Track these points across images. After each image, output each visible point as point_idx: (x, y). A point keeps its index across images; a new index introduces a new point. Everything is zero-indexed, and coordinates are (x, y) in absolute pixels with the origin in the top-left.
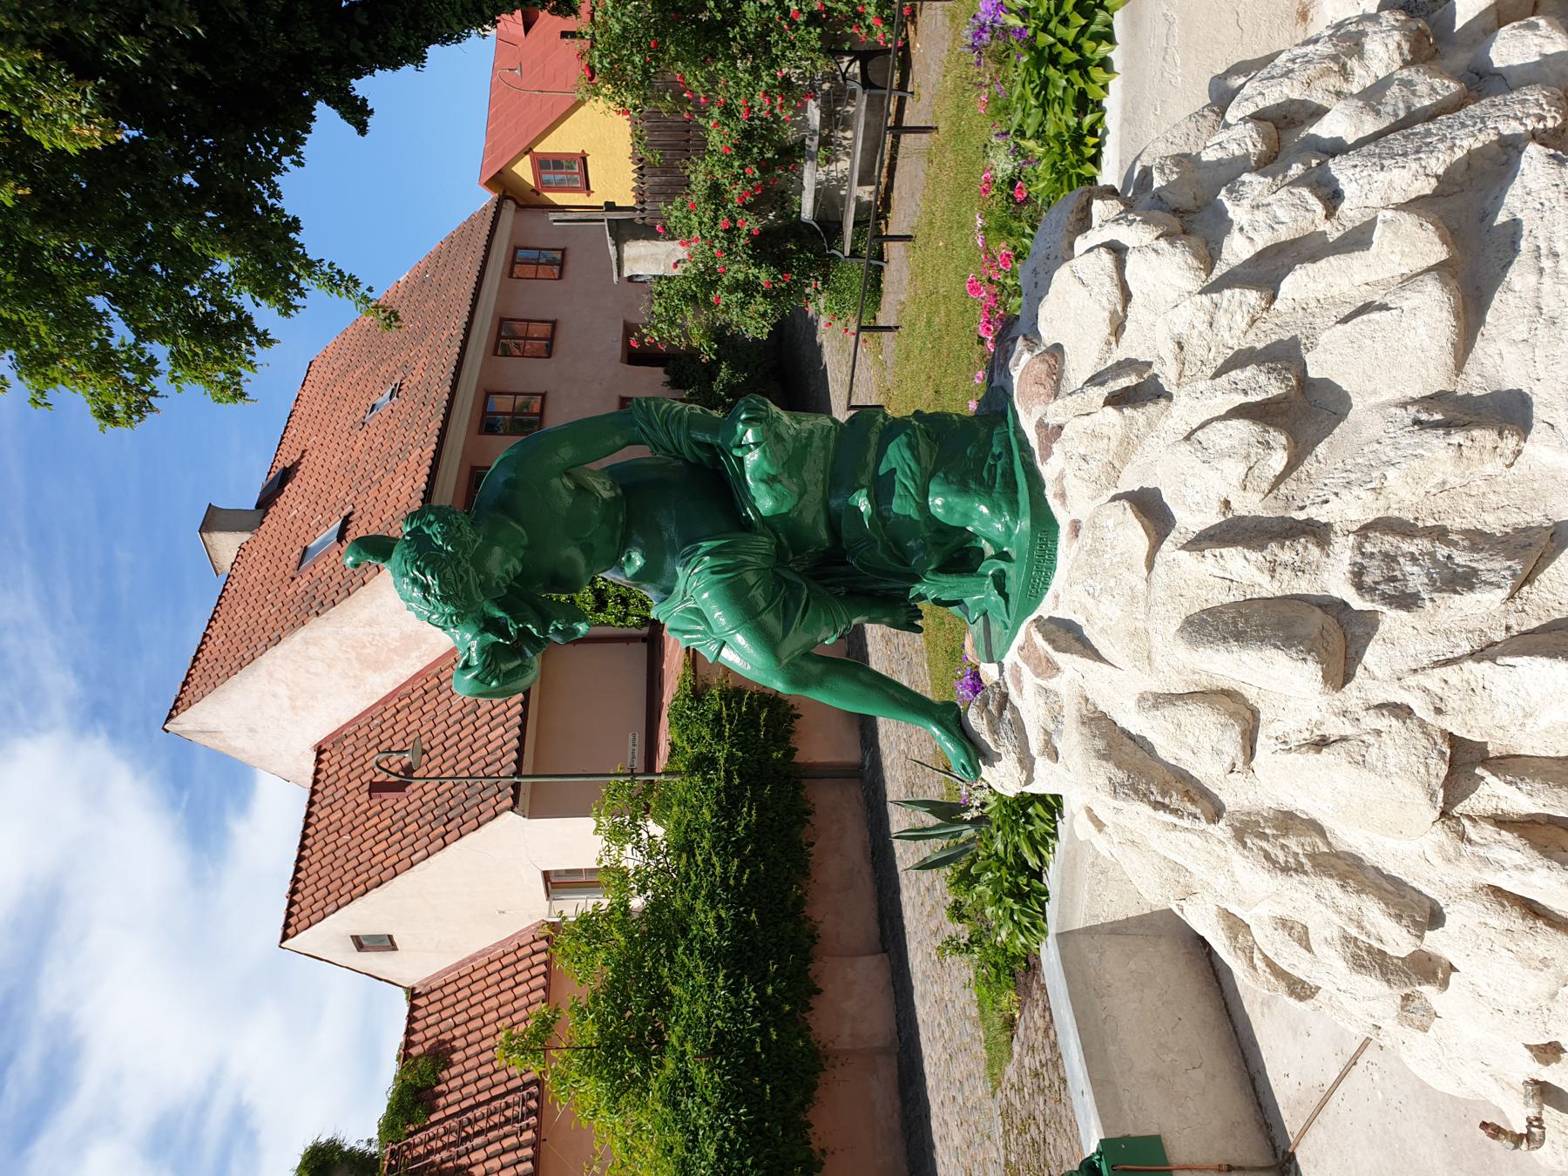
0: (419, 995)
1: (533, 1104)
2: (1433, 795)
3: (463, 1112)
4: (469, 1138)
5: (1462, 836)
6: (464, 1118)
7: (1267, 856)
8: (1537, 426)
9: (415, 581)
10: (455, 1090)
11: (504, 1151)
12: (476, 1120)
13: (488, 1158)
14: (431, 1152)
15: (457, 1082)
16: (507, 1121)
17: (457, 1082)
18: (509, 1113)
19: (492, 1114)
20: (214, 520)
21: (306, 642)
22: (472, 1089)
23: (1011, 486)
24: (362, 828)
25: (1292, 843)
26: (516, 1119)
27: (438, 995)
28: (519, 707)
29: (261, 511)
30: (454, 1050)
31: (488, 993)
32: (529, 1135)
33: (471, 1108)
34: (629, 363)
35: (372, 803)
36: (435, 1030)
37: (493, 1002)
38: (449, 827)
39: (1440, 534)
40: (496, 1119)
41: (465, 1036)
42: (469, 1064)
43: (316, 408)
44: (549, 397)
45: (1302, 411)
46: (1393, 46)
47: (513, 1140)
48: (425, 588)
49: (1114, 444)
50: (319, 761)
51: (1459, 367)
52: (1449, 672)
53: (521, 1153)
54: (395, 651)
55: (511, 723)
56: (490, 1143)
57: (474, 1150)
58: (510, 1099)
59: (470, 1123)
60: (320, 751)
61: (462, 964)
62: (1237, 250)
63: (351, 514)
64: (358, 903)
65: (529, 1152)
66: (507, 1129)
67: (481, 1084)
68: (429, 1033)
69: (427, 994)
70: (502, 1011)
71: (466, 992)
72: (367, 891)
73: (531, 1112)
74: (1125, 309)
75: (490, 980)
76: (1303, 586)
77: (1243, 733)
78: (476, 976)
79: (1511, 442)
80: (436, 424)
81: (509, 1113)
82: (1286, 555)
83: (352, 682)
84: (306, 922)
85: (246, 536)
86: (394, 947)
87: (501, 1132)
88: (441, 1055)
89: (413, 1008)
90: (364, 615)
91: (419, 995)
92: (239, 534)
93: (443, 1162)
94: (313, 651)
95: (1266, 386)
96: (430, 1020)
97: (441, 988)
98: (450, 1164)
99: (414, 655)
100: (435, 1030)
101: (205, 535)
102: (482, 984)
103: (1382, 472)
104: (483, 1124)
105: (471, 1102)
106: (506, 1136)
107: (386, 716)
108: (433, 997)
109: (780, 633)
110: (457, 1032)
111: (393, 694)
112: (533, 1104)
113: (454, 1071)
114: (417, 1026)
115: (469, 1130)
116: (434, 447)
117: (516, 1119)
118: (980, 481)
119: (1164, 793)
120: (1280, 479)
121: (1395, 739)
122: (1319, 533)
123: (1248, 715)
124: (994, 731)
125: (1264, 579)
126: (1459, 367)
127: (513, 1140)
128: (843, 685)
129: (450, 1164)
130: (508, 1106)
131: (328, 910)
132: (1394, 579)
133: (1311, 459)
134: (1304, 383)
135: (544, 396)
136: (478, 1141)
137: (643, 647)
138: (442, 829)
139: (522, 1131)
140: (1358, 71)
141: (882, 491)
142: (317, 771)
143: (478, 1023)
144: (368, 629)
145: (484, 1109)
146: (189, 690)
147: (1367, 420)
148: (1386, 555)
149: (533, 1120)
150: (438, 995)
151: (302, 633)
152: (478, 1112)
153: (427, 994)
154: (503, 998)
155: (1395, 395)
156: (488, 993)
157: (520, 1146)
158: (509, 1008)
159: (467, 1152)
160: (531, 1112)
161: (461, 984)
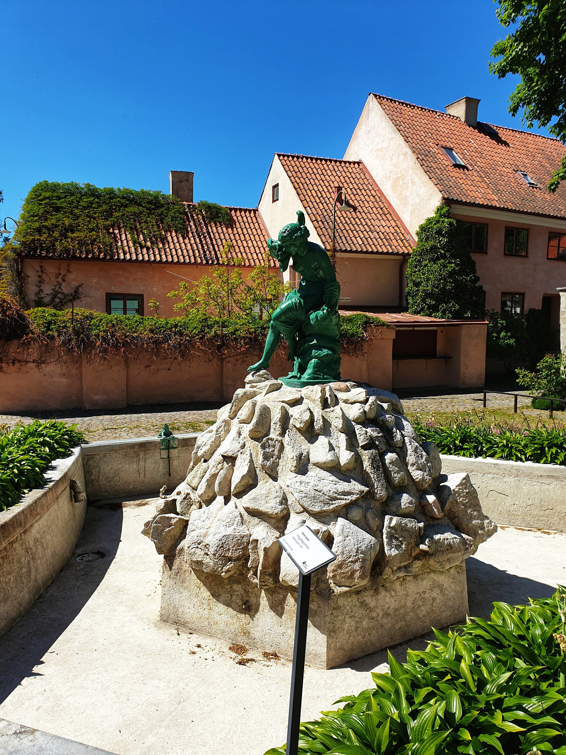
0: (255, 213)
1: (210, 262)
2: (226, 453)
3: (209, 234)
4: (199, 236)
5: (219, 463)
6: (206, 234)
7: (220, 427)
8: (296, 475)
9: (286, 230)
10: (218, 232)
11: (193, 251)
12: (205, 240)
13: (191, 245)
14: (194, 220)
15: (220, 231)
16: (204, 252)
17: (220, 231)
18: (208, 252)
19: (207, 246)
20: (472, 104)
21: (405, 154)
22: (217, 237)
23: (314, 378)
24: (350, 176)
25: (223, 432)
26: (205, 255)
27: (255, 221)
28: (370, 250)
29: (476, 125)
30: (232, 229)
31: (254, 242)
32: (199, 261)
33: (210, 237)
34: (544, 297)
35: (333, 188)
36: (241, 220)
37: (250, 244)
38: (320, 223)
39: (279, 457)
40: (206, 247)
41: (238, 233)
42: (227, 235)
43: (530, 146)
44: (525, 259)
45: (310, 432)
46: (418, 476)
47: (197, 254)
48: (284, 232)
49: (314, 397)
50: (354, 163)
51: (314, 464)
52: (249, 455)
53: (175, 257)
54: (401, 194)
55: (353, 247)
56: (197, 245)
57: (195, 239)
58: (213, 253)
59: (205, 237)
60: (359, 163)
61: (266, 231)
62: (357, 427)
63: (468, 170)
64: (291, 185)
65: (193, 261)
66: (202, 252)
67: (219, 240)
68: (240, 218)
69: (255, 216)
70: (247, 248)
71: (255, 233)
72: (296, 189)
73: (207, 261)
74: (350, 403)
75: (259, 243)
76: (272, 430)
77: (244, 420)
78: (261, 237)
79: (293, 469)
80: (510, 206)
81: (208, 252)
82: (278, 426)
83: (388, 175)
84: (285, 164)
85: (463, 119)
86: (274, 201)
87: (200, 250)
88: (231, 224)
89: (250, 211)
90: (417, 179)
91: (255, 213)
92: (464, 116)
93: (191, 227)
94: (402, 157)
95: (318, 425)
96: (245, 218)
97: (257, 222)
98: (189, 229)
99: (398, 202)
100: (241, 220)
101: (464, 100)
102: (258, 239)
103: (293, 446)
104: (204, 242)
105: (212, 237)
106: (199, 252)
107: (373, 192)
108: (254, 219)
109: (282, 320)
110: (239, 230)
111: (382, 194)
112: (210, 262)
113: (224, 229)
114: (243, 213)
115: (202, 236)
116: (498, 206)
117: (205, 255)
118: (316, 371)
119: (235, 405)
120: (295, 427)
121: (237, 446)
122: (283, 434)
123: (248, 422)
124: (259, 375)
125: (274, 422)
126: (314, 464)
127: (197, 254)
128: (272, 338)
129: (189, 229)
130: (210, 252)
131: (289, 173)
132: (269, 446)
133: (300, 435)
134: (318, 435)
135: (526, 256)
136: (198, 240)
137: (397, 304)
138: (320, 219)
139: (201, 258)
140: (413, 468)
141: (318, 347)
142: (350, 163)
143: (243, 239)
144: (410, 181)
145: (210, 242)
146: (389, 103)
147: (305, 446)
148: (275, 446)
149: (204, 262)
150: (255, 221)
151: (409, 151)
152: (208, 240)
153: (255, 216)
154: (252, 248)
155: (311, 452)
156: (254, 242)
157: (195, 258)
158: (248, 251)
159: (194, 236)
160: (207, 261)
161: (259, 231)
